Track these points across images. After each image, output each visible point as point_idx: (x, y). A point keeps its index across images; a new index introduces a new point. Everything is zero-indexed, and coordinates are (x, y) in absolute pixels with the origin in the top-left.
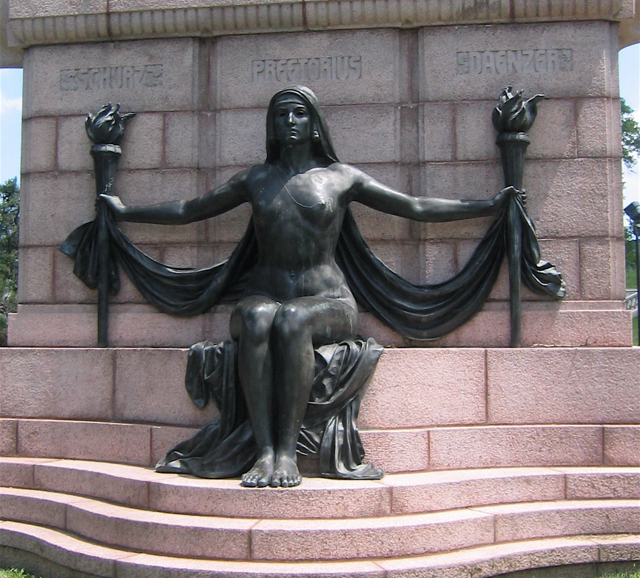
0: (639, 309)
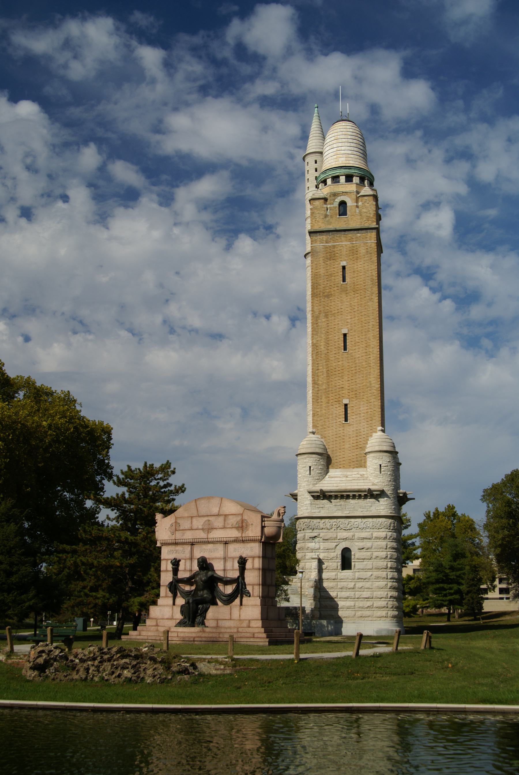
0: (195, 588)
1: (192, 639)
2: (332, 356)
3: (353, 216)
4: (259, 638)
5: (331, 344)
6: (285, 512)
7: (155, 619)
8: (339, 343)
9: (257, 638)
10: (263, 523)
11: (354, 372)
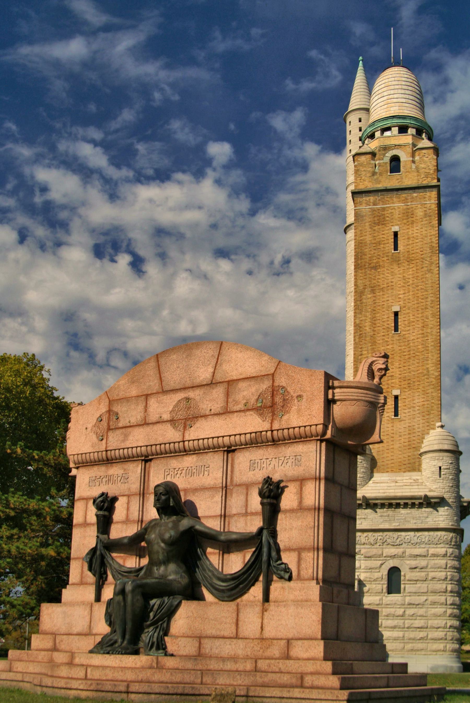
1: (123, 688)
2: (378, 338)
3: (408, 173)
4: (318, 688)
5: (378, 325)
6: (386, 369)
7: (52, 634)
8: (389, 323)
9: (312, 687)
10: (330, 391)
11: (407, 357)
